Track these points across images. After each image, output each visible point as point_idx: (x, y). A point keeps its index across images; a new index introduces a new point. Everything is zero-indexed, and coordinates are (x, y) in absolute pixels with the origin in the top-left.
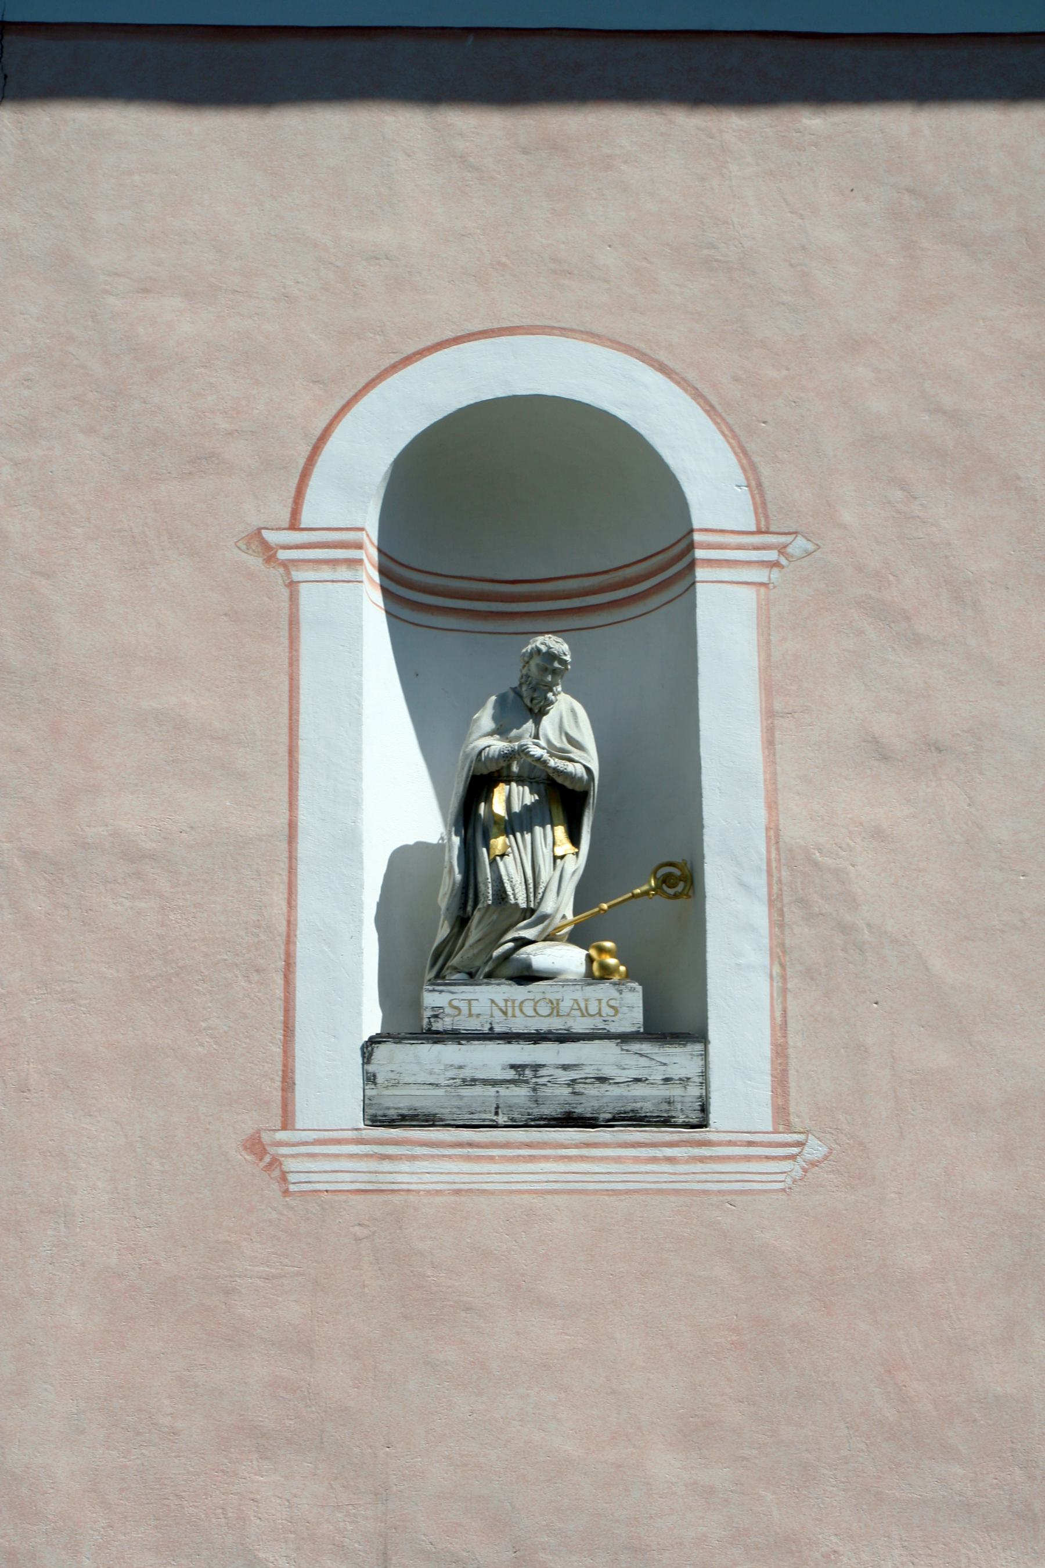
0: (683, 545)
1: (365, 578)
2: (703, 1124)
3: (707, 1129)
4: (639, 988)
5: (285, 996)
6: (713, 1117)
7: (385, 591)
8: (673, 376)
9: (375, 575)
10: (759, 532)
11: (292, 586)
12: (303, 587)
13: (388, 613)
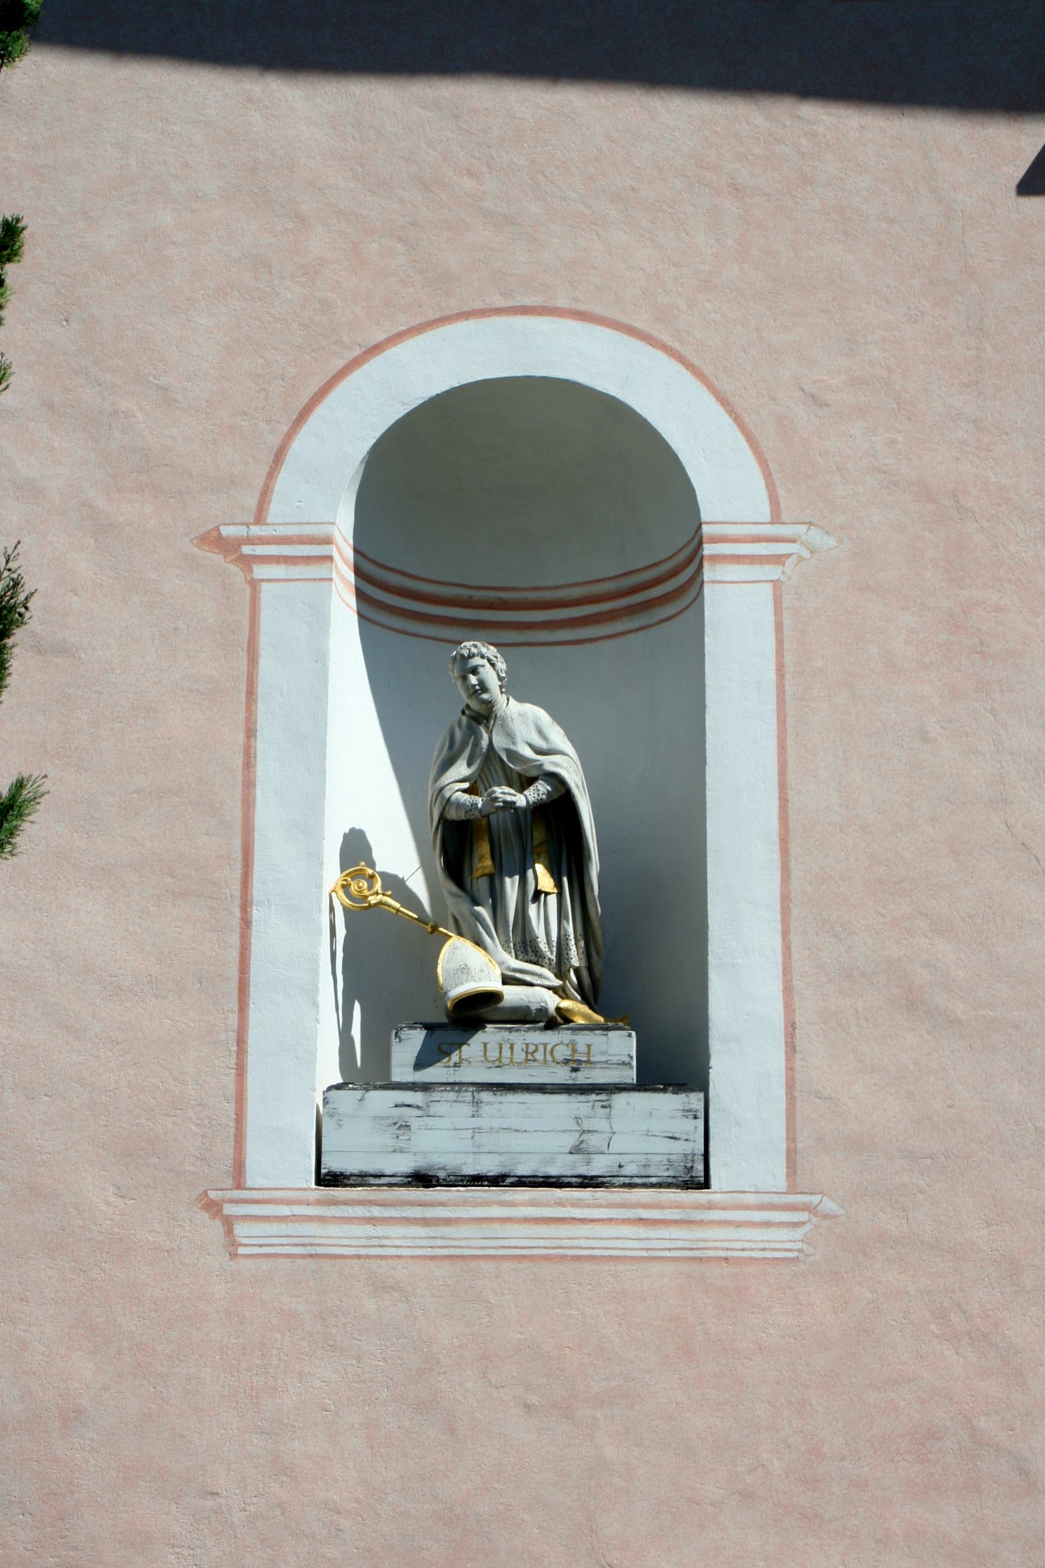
0: (690, 549)
1: (334, 576)
2: (706, 1185)
3: (709, 1190)
4: (634, 1033)
5: (239, 1028)
6: (713, 1181)
7: (360, 595)
8: (579, 1180)
9: (351, 576)
10: (772, 523)
11: (254, 585)
12: (265, 587)
13: (360, 615)
